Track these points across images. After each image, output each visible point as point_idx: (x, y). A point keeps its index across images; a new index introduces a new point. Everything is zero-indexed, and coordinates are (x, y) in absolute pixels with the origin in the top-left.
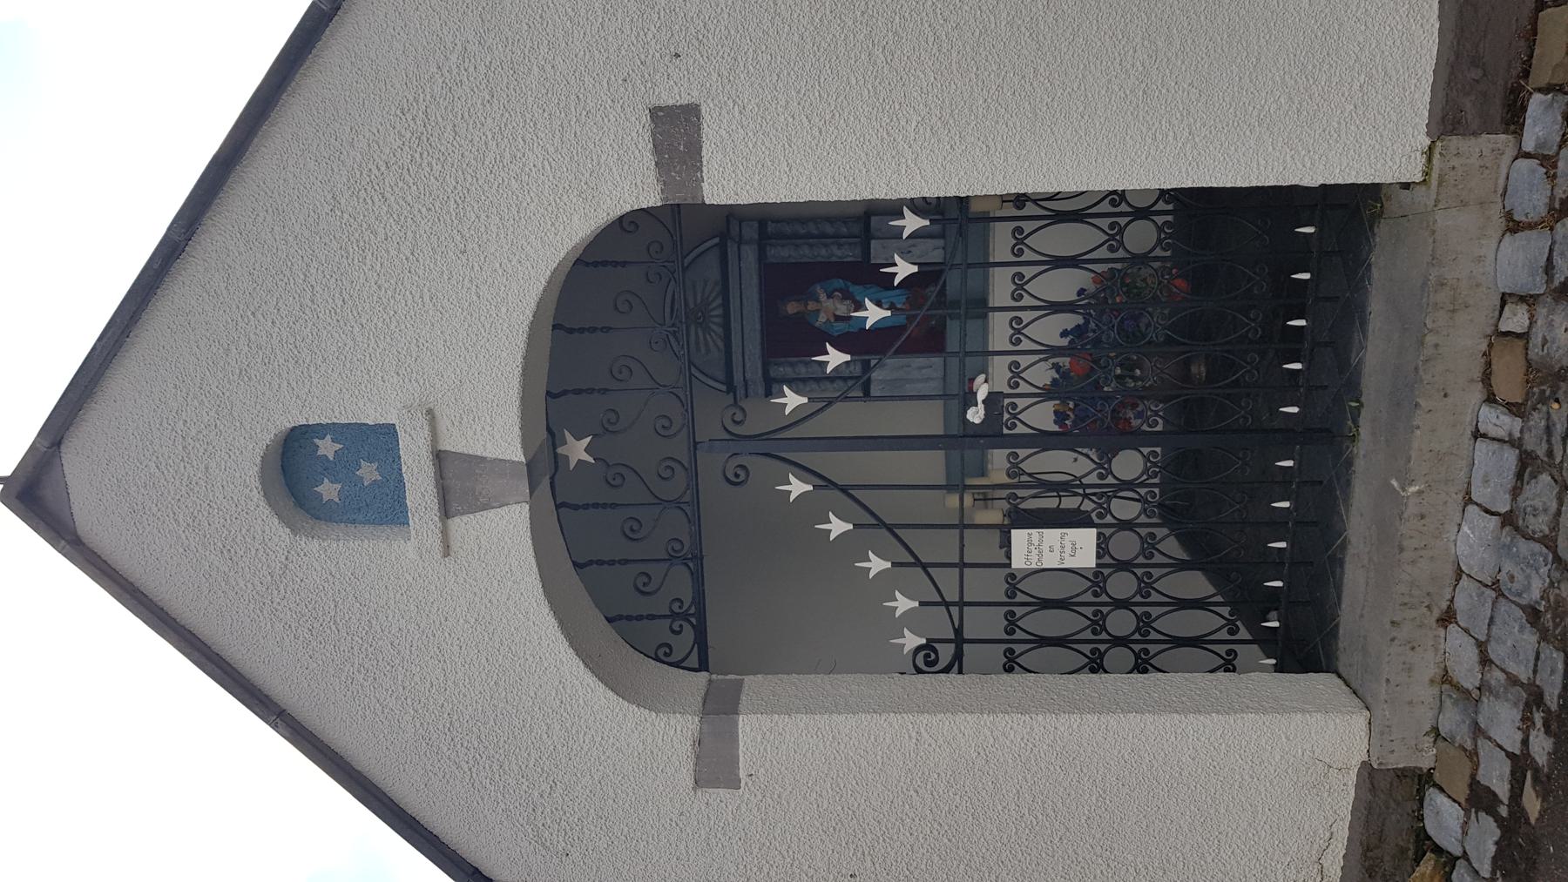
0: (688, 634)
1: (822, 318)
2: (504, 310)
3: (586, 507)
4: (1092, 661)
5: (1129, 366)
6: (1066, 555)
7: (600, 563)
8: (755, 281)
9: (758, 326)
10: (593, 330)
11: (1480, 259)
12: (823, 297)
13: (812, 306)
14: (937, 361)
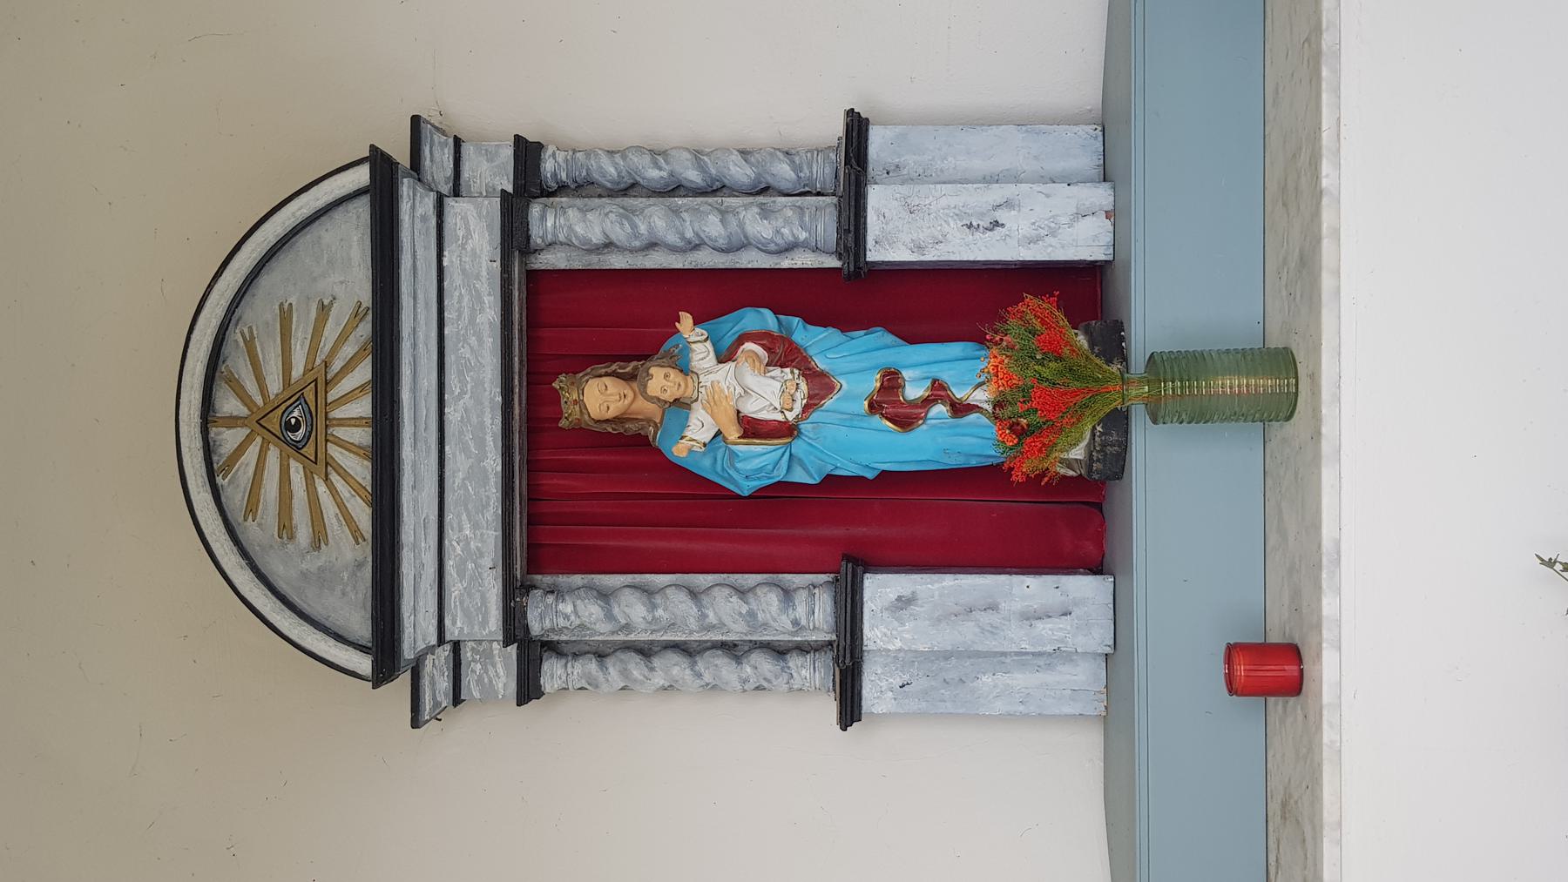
1: (700, 427)
5: (796, 623)
8: (491, 313)
13: (661, 381)
14: (1085, 589)
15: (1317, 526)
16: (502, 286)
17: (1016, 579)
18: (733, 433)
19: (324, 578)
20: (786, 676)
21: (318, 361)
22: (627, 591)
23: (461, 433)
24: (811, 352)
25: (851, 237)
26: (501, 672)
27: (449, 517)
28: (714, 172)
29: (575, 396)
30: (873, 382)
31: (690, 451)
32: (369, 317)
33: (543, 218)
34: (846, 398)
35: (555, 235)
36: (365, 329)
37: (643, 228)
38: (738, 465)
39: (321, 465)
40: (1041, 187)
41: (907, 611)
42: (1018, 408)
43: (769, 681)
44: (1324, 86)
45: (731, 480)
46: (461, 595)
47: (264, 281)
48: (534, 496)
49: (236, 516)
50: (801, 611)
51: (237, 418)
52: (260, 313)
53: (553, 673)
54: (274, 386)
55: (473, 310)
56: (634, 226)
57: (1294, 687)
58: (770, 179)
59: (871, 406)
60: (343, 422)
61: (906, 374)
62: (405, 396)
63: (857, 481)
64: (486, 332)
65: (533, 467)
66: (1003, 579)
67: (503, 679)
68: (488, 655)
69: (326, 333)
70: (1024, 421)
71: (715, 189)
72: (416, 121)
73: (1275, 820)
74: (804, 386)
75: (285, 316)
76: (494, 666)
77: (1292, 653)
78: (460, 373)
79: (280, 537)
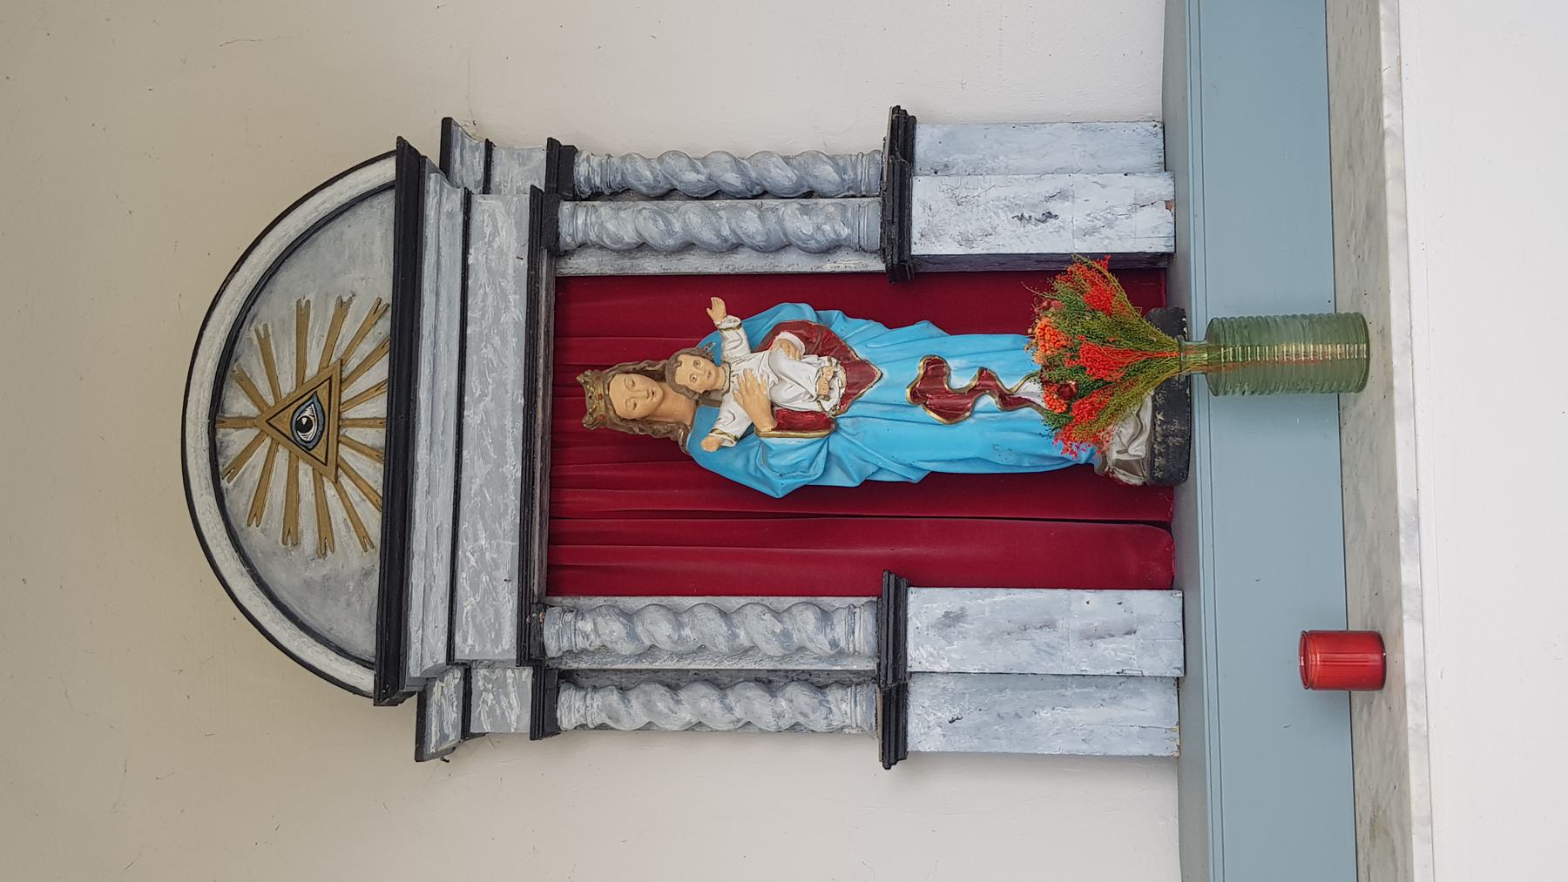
1: (731, 420)
5: (834, 644)
8: (516, 313)
13: (689, 369)
14: (1151, 606)
15: (1393, 490)
16: (528, 283)
17: (1075, 594)
18: (766, 425)
19: (329, 588)
20: (824, 711)
21: (334, 359)
22: (652, 609)
23: (481, 437)
24: (850, 343)
25: (894, 229)
26: (514, 703)
27: (464, 526)
28: (754, 175)
29: (600, 391)
30: (918, 370)
31: (721, 447)
32: (389, 314)
33: (574, 215)
34: (887, 386)
35: (586, 233)
36: (384, 326)
37: (677, 226)
38: (772, 461)
39: (329, 468)
40: (1097, 178)
41: (953, 628)
42: (1064, 371)
43: (806, 716)
44: (1382, 24)
45: (765, 480)
46: (474, 610)
47: (283, 277)
48: (555, 514)
49: (240, 520)
50: (840, 631)
51: (246, 418)
52: (276, 310)
53: (571, 707)
54: (287, 385)
55: (497, 308)
56: (668, 223)
57: (1376, 678)
58: (812, 181)
59: (913, 394)
60: (356, 423)
61: (952, 363)
62: (423, 395)
63: (902, 487)
64: (511, 331)
65: (556, 483)
66: (1061, 593)
67: (517, 710)
68: (501, 685)
69: (343, 330)
70: (1077, 397)
71: (759, 193)
72: (447, 123)
73: (1365, 844)
74: (842, 375)
75: (302, 314)
76: (507, 696)
77: (1375, 641)
78: (482, 374)
79: (285, 543)
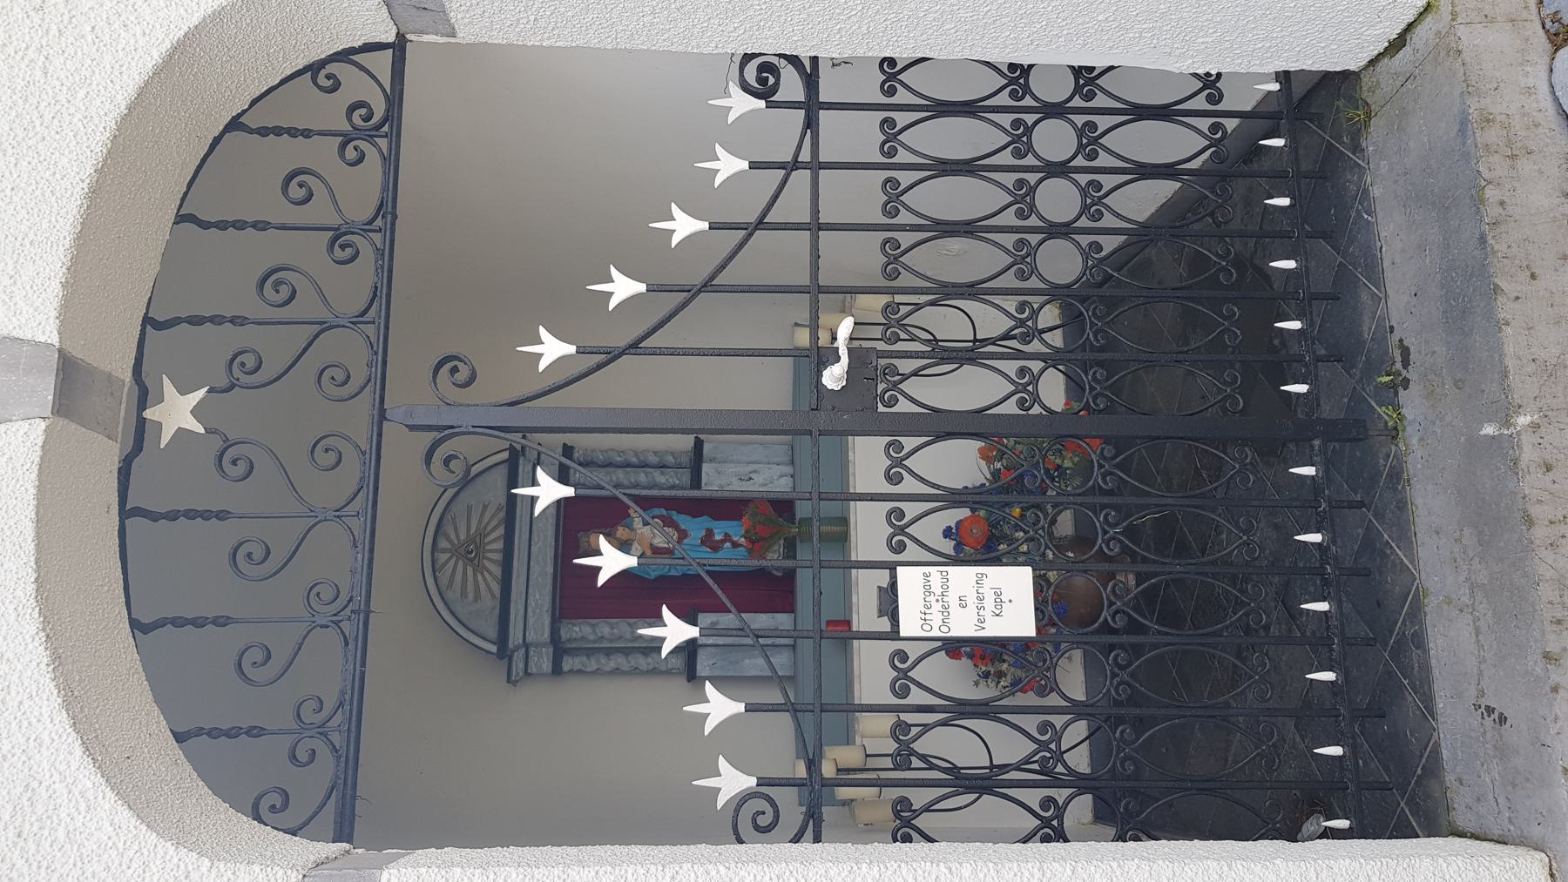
0: (325, 768)
2: (81, 94)
3: (172, 516)
4: (1046, 822)
6: (987, 613)
7: (179, 622)
9: (550, 569)
10: (239, 225)
11: (1529, 91)
12: (638, 523)
